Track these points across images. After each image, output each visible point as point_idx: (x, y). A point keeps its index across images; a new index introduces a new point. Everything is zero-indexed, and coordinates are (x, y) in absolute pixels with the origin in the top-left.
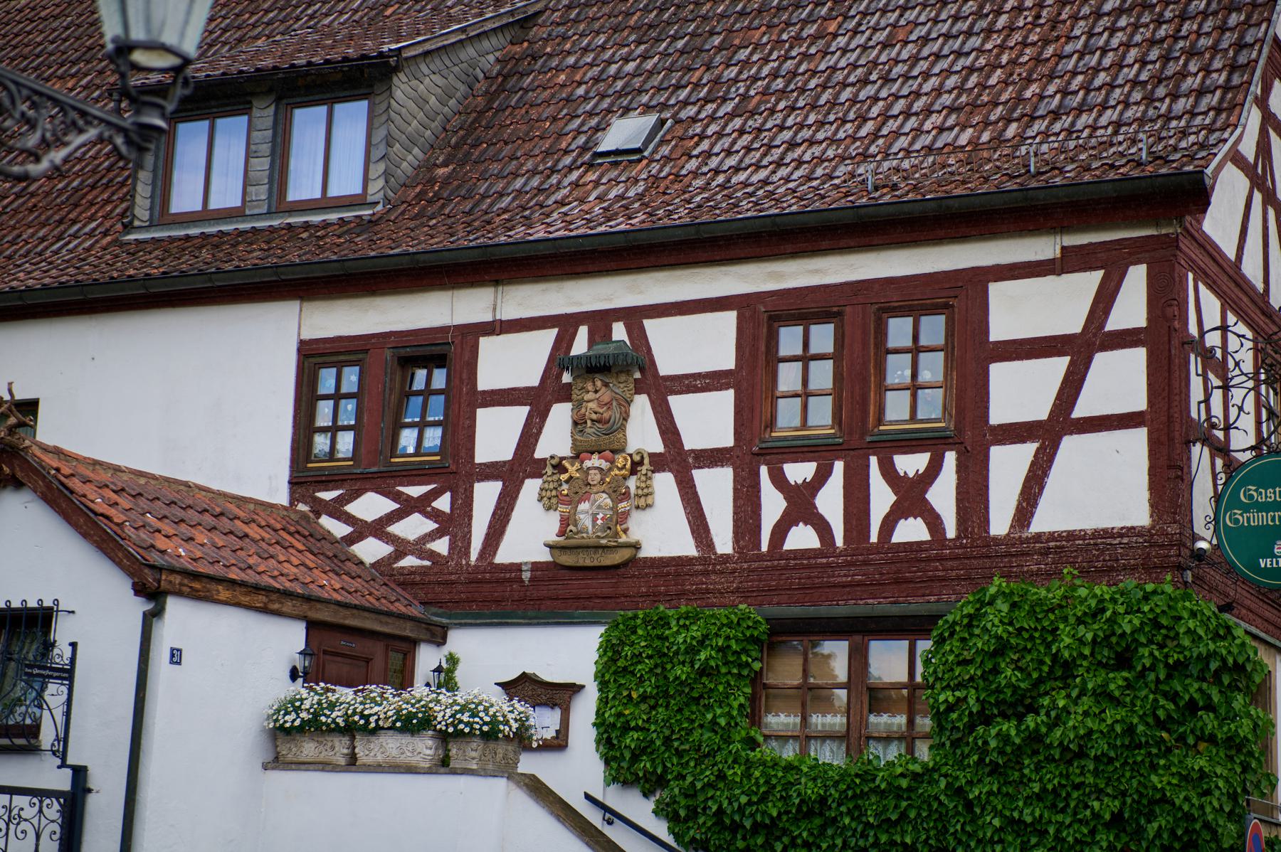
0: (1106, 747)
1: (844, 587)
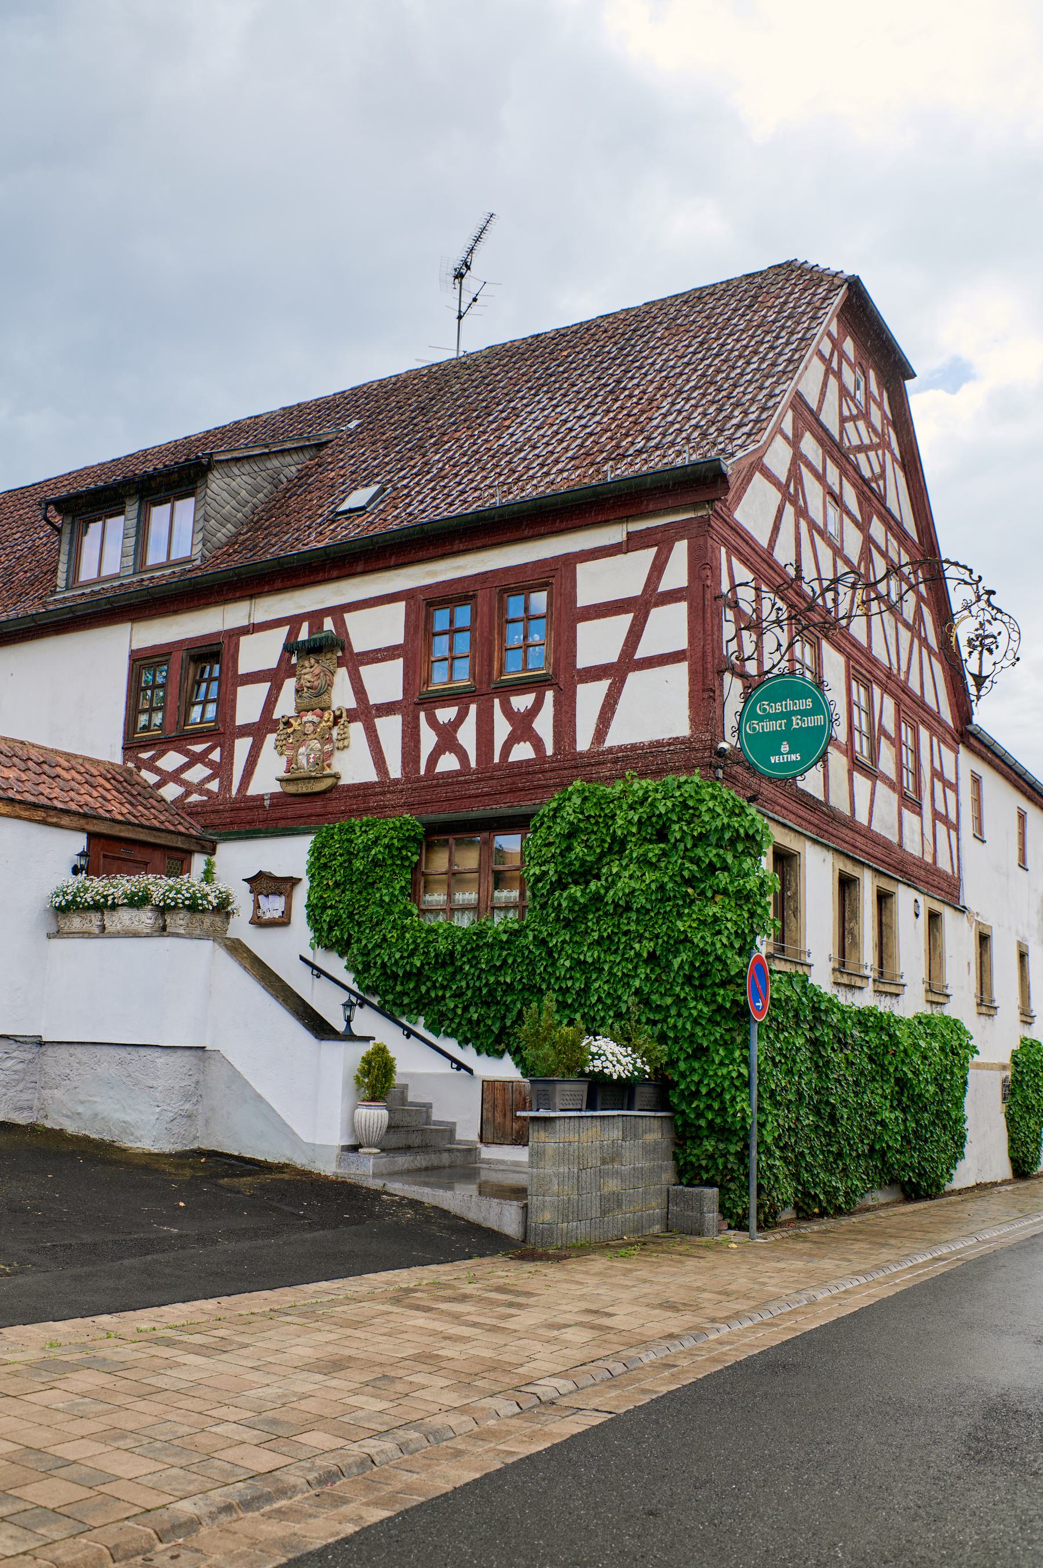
0: (644, 901)
1: (477, 797)
